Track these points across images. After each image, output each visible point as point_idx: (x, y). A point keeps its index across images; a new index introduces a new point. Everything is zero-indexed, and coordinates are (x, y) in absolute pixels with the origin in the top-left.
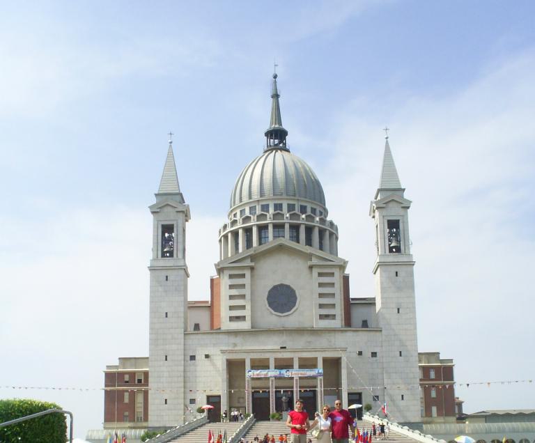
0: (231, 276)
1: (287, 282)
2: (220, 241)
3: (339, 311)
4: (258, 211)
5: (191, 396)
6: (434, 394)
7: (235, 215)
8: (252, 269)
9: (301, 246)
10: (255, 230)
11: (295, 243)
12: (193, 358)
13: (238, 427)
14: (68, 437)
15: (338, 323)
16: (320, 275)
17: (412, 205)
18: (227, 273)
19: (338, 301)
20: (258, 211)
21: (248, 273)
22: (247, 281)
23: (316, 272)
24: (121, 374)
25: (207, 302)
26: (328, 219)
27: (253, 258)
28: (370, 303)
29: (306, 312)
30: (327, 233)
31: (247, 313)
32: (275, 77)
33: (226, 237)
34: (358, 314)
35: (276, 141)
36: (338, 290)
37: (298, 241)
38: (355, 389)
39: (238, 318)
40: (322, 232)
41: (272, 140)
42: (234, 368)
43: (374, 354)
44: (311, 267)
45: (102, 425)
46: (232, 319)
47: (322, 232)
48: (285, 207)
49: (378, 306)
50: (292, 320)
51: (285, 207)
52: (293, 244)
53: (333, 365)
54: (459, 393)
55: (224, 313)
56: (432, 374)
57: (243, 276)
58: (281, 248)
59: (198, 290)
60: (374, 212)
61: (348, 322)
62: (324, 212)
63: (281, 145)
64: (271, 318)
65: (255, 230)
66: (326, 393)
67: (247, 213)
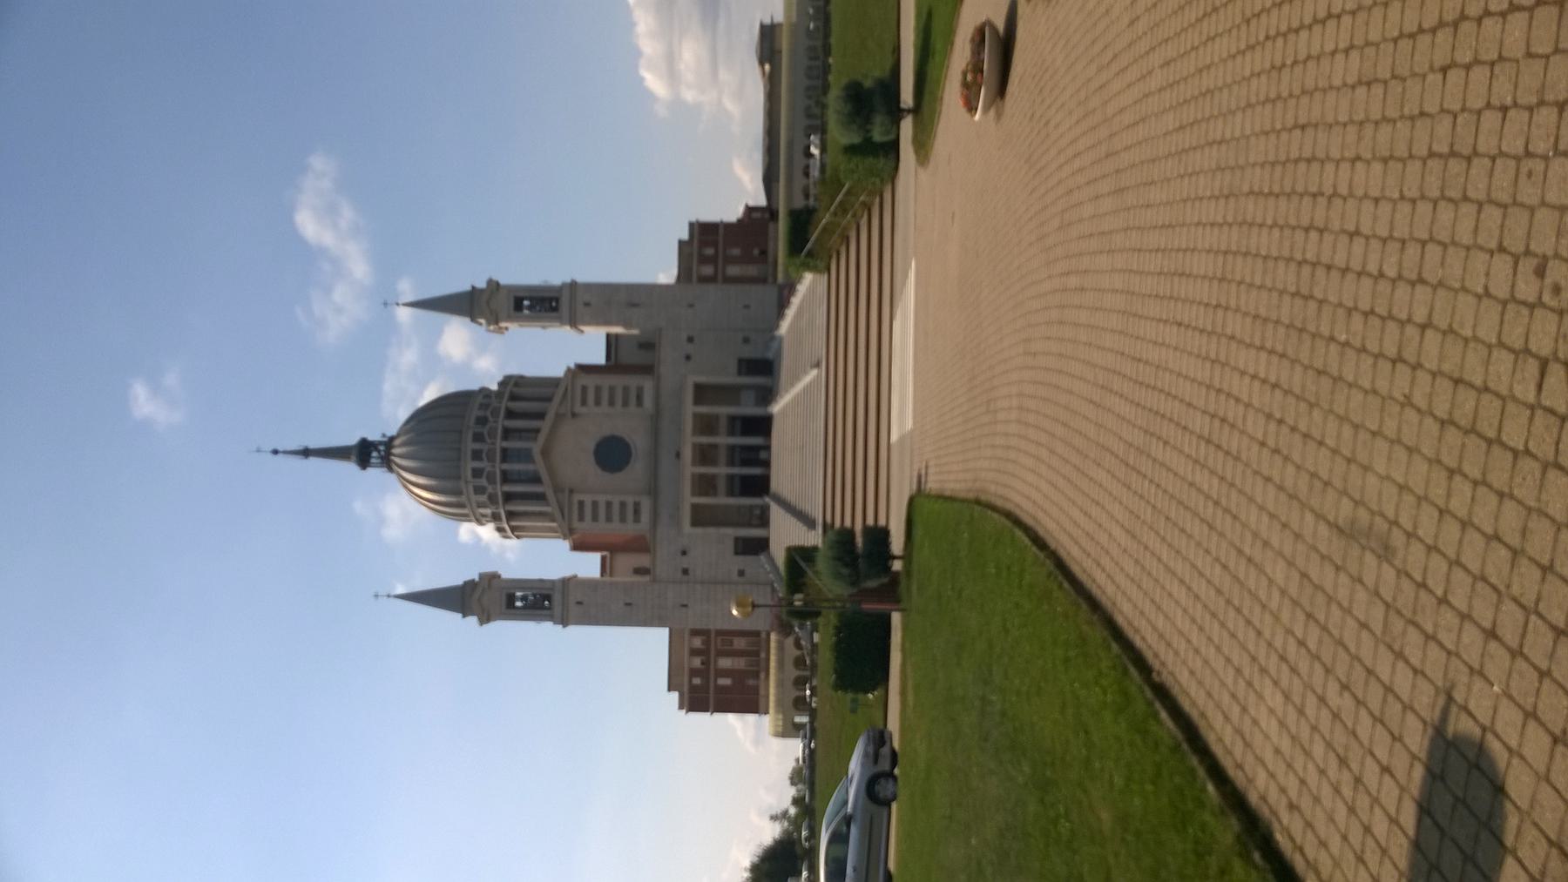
0: (581, 518)
1: (592, 446)
2: (518, 537)
3: (633, 381)
4: (483, 482)
5: (735, 576)
6: (736, 252)
7: (483, 516)
8: (571, 491)
9: (545, 425)
10: (507, 488)
11: (540, 435)
12: (685, 572)
13: (776, 513)
14: (907, 97)
15: (648, 384)
16: (584, 402)
17: (495, 278)
18: (576, 524)
19: (607, 381)
20: (483, 482)
21: (577, 498)
22: (588, 499)
23: (578, 409)
24: (693, 688)
25: (603, 559)
26: (494, 387)
27: (558, 489)
28: (612, 342)
29: (630, 426)
30: (517, 390)
31: (630, 500)
32: (275, 452)
33: (513, 529)
34: (629, 356)
35: (375, 454)
36: (591, 381)
37: (537, 431)
38: (733, 367)
39: (637, 512)
40: (513, 398)
41: (373, 461)
42: (701, 518)
43: (690, 340)
44: (574, 415)
45: (763, 716)
46: (637, 519)
47: (513, 398)
48: (477, 446)
49: (617, 330)
50: (639, 441)
51: (477, 446)
52: (542, 438)
53: (703, 393)
54: (732, 213)
55: (630, 529)
56: (709, 251)
57: (581, 504)
58: (546, 453)
59: (588, 565)
60: (500, 328)
61: (647, 369)
62: (484, 392)
63: (382, 448)
64: (637, 470)
65: (507, 488)
66: (737, 403)
67: (484, 498)
